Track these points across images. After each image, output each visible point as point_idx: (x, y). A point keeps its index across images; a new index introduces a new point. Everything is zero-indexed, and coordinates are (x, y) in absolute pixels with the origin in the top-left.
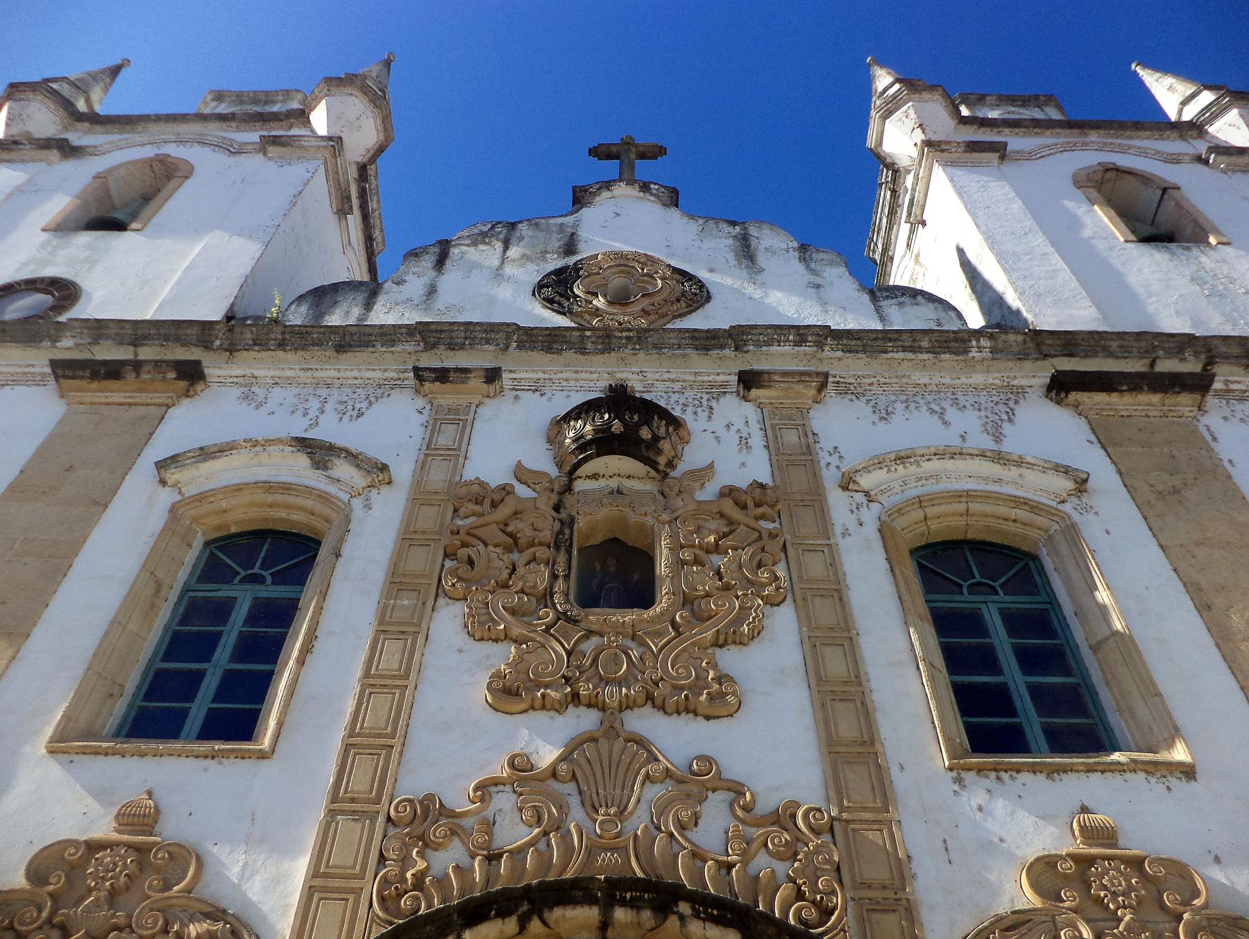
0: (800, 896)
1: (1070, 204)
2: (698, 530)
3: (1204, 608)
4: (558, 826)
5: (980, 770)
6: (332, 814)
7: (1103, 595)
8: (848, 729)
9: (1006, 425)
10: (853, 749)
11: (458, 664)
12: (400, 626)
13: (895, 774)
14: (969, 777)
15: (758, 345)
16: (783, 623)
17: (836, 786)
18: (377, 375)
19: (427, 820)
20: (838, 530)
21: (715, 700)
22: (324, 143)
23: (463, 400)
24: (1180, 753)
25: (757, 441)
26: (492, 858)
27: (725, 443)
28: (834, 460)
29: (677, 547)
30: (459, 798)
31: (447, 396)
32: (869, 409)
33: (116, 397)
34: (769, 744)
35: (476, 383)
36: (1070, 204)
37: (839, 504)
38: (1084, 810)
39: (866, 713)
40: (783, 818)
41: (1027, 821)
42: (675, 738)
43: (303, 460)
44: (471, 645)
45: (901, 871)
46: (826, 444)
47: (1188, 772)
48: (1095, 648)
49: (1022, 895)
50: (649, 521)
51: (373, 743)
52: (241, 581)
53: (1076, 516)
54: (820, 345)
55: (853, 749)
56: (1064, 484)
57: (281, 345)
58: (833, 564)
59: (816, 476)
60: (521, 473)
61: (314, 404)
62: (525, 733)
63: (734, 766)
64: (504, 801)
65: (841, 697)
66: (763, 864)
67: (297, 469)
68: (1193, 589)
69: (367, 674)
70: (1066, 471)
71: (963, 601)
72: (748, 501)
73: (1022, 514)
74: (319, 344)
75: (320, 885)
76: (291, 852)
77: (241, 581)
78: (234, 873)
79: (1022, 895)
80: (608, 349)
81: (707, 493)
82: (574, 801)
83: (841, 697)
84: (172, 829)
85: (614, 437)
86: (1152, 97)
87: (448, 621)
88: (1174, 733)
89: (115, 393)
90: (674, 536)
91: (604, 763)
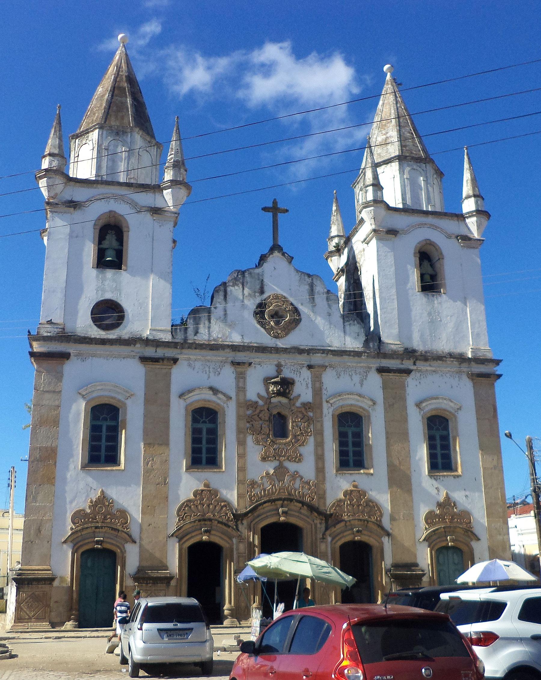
0: (310, 496)
1: (409, 267)
2: (297, 417)
3: (387, 438)
4: (274, 485)
5: (340, 473)
6: (238, 484)
7: (370, 435)
8: (320, 465)
9: (365, 381)
10: (320, 470)
11: (254, 451)
12: (241, 443)
13: (326, 474)
14: (338, 475)
15: (313, 354)
16: (311, 440)
17: (317, 477)
18: (220, 358)
19: (253, 484)
20: (324, 415)
21: (299, 459)
22: (173, 215)
23: (243, 370)
24: (372, 471)
25: (310, 385)
26: (265, 491)
27: (303, 391)
28: (325, 392)
29: (293, 422)
30: (258, 480)
31: (240, 369)
32: (335, 373)
33: (158, 367)
34: (307, 469)
35: (247, 365)
36: (409, 267)
37: (325, 405)
38: (354, 481)
39: (323, 449)
40: (308, 483)
41: (345, 483)
42: (292, 467)
43: (211, 392)
44: (254, 446)
45: (325, 492)
46: (324, 387)
47: (372, 474)
48: (366, 445)
49: (342, 496)
50: (287, 413)
51: (242, 469)
52: (202, 422)
53: (371, 411)
54: (327, 354)
55: (320, 470)
56: (371, 403)
57: (196, 348)
58: (322, 426)
59: (321, 398)
60: (259, 396)
61: (207, 369)
62: (267, 466)
63: (301, 473)
64: (265, 480)
65: (320, 458)
66: (306, 491)
67: (209, 395)
68: (387, 433)
69: (238, 454)
70: (372, 400)
71: (199, 426)
72: (307, 406)
73: (361, 410)
74: (204, 349)
75: (240, 496)
76: (233, 490)
77: (202, 422)
78: (225, 494)
79: (342, 496)
80: (277, 353)
81: (298, 404)
82: (276, 480)
83: (320, 458)
84: (213, 486)
85: (281, 392)
86: (463, 175)
87: (250, 440)
88: (372, 467)
89: (157, 366)
90: (292, 419)
91: (281, 471)
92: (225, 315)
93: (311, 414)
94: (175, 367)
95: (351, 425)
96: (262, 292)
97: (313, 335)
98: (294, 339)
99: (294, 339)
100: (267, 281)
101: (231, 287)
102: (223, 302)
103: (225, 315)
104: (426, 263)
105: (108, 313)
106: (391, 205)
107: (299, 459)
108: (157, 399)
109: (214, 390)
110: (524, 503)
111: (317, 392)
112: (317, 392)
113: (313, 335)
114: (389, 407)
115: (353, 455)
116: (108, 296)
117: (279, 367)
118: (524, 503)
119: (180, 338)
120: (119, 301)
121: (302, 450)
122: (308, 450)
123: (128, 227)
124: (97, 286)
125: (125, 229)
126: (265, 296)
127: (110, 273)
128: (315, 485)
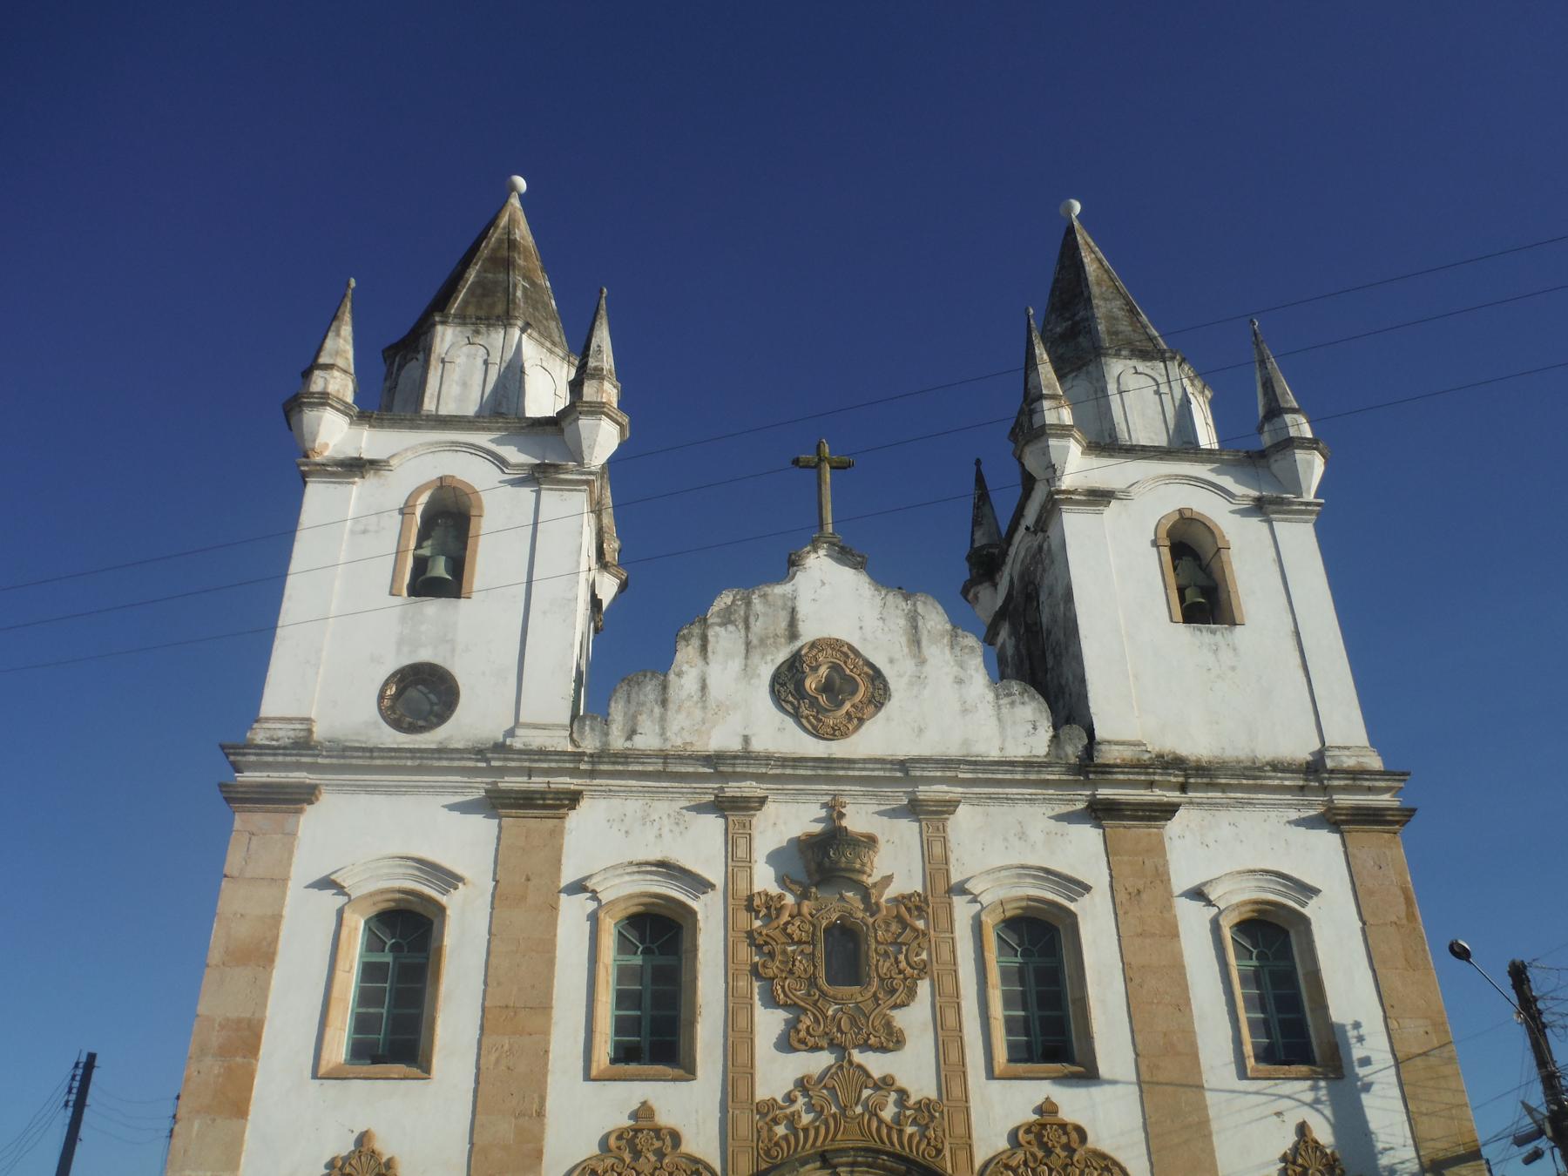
10: (949, 1067)
21: (893, 1041)
27: (896, 862)
42: (876, 1064)
63: (902, 1082)
72: (913, 905)
92: (704, 687)
93: (920, 924)
94: (572, 813)
95: (1040, 940)
96: (793, 634)
97: (921, 730)
98: (875, 739)
99: (875, 739)
100: (804, 609)
101: (717, 629)
102: (700, 663)
103: (704, 687)
104: (1186, 562)
105: (422, 692)
106: (551, 413)
107: (893, 1041)
108: (525, 894)
109: (667, 868)
110: (666, 740)
111: (935, 864)
112: (935, 864)
113: (921, 730)
114: (1124, 900)
115: (1050, 1031)
116: (425, 655)
117: (834, 810)
118: (666, 740)
119: (590, 744)
120: (447, 666)
121: (900, 1018)
122: (915, 1018)
123: (480, 507)
124: (403, 632)
125: (474, 512)
126: (798, 644)
127: (433, 607)
128: (844, 1049)
